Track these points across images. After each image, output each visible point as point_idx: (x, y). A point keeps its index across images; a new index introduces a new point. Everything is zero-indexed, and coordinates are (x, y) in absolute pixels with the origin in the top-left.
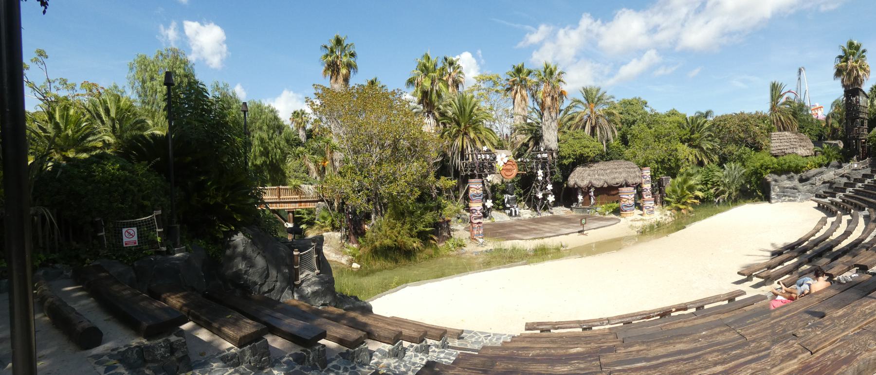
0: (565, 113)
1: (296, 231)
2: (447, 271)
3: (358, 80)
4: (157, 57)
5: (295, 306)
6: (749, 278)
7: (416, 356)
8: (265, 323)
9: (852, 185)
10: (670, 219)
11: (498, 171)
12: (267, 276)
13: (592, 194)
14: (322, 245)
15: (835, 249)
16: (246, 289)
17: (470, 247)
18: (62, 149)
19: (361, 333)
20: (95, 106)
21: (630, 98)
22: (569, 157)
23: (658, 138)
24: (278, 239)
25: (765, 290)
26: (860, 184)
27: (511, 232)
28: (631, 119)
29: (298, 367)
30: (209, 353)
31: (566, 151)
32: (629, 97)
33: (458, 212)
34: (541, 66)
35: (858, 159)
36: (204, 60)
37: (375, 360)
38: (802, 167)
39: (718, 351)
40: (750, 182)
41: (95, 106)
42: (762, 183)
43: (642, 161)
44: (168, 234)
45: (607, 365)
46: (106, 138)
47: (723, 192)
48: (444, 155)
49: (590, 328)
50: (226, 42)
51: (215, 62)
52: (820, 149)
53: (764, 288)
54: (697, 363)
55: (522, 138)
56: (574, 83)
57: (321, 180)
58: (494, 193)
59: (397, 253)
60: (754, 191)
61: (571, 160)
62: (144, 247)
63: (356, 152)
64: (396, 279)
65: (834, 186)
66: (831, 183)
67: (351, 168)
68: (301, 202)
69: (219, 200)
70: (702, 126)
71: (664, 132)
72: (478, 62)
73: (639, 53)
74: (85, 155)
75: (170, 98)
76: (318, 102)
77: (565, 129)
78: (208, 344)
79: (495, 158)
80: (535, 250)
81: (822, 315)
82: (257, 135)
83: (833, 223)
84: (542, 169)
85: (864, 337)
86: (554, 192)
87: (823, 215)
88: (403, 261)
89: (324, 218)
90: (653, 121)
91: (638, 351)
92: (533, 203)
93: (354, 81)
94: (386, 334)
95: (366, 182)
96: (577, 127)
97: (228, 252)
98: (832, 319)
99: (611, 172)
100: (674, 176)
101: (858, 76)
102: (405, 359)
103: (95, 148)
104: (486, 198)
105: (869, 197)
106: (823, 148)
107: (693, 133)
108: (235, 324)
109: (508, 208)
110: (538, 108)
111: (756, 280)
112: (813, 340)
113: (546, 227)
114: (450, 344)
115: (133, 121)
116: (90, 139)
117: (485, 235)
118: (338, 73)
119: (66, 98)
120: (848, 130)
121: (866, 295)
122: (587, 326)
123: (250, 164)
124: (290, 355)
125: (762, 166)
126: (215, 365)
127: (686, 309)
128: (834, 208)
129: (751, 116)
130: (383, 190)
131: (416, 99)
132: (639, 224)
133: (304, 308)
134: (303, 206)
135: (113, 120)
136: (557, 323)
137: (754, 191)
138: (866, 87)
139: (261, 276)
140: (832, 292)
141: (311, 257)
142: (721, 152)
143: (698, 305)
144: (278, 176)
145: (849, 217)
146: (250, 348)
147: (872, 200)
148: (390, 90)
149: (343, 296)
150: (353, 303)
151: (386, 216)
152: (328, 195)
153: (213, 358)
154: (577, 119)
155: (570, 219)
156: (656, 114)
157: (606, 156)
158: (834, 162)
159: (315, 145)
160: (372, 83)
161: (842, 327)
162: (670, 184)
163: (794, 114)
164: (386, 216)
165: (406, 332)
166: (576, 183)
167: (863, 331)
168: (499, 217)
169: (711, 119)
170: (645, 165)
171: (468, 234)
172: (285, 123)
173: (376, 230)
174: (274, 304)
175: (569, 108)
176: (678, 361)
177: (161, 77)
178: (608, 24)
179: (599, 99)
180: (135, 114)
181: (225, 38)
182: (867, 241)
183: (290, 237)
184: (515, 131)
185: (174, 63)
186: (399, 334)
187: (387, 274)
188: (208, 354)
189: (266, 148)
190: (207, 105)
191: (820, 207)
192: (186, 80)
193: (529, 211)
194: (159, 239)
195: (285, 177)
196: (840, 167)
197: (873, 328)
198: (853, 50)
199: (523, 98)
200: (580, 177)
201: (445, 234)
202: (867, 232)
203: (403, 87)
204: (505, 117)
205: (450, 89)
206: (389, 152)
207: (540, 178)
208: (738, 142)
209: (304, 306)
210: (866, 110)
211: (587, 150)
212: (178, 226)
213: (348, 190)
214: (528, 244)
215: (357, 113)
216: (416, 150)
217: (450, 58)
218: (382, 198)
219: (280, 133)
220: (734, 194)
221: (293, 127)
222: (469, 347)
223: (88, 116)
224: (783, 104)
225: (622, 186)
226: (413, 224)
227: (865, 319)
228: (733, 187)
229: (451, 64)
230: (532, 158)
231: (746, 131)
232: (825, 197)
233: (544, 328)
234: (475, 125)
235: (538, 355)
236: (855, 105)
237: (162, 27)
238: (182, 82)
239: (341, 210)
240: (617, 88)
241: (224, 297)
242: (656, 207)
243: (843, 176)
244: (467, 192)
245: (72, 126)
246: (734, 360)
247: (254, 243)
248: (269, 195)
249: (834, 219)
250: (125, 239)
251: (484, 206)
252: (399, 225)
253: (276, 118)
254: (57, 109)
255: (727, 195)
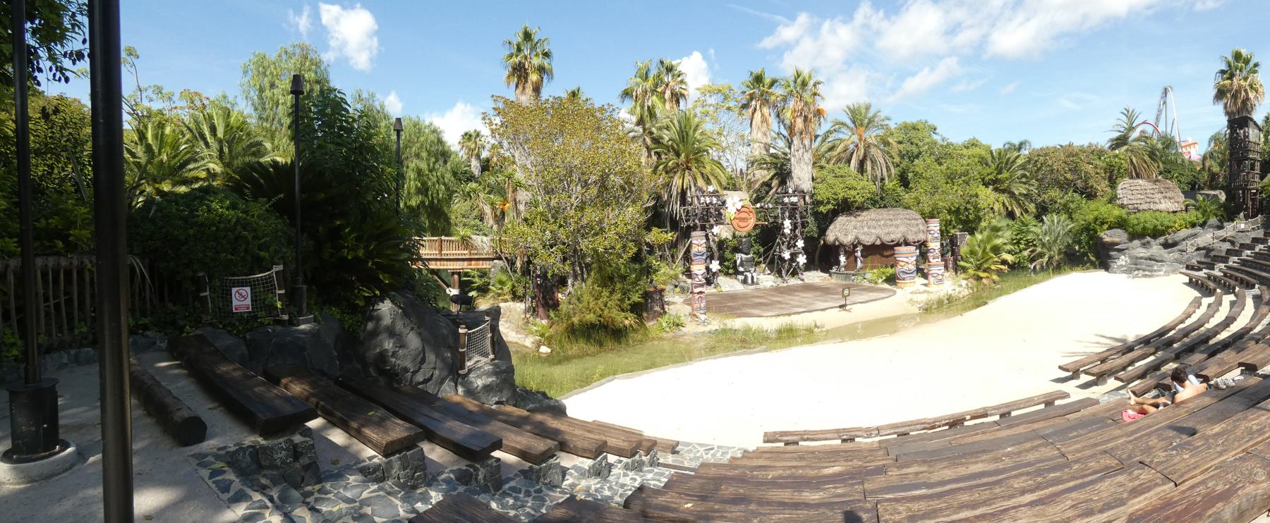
0: (824, 140)
1: (463, 300)
2: (658, 360)
3: (552, 91)
4: (280, 56)
5: (458, 404)
6: (1076, 374)
7: (625, 475)
8: (420, 426)
9: (1237, 253)
10: (966, 292)
11: (728, 221)
12: (423, 361)
13: (859, 254)
14: (498, 320)
15: (1211, 342)
16: (393, 376)
17: (690, 328)
18: (155, 180)
19: (550, 443)
20: (197, 122)
21: (915, 121)
22: (828, 203)
23: (951, 178)
24: (438, 311)
25: (1095, 392)
26: (1249, 252)
27: (745, 306)
28: (916, 151)
29: (461, 489)
30: (344, 464)
31: (824, 194)
32: (912, 119)
33: (676, 277)
34: (790, 73)
35: (1246, 217)
36: (347, 59)
37: (569, 481)
38: (1168, 227)
39: (1028, 474)
40: (1079, 243)
41: (197, 122)
42: (1096, 244)
43: (927, 210)
44: (291, 298)
45: (873, 492)
46: (211, 166)
47: (1041, 255)
48: (658, 197)
49: (852, 440)
50: (377, 33)
51: (362, 60)
52: (1193, 202)
53: (1095, 388)
54: (997, 490)
55: (763, 175)
56: (836, 100)
57: (499, 229)
58: (722, 252)
59: (602, 333)
60: (1085, 254)
61: (830, 206)
62: (260, 314)
63: (549, 192)
64: (601, 368)
65: (1212, 254)
66: (1208, 250)
67: (542, 214)
68: (470, 260)
69: (361, 253)
70: (1014, 162)
71: (960, 170)
72: (710, 67)
73: (932, 59)
74: (183, 189)
75: (297, 111)
76: (498, 120)
77: (823, 163)
78: (343, 450)
79: (724, 203)
80: (779, 332)
81: (1193, 433)
82: (412, 165)
83: (1209, 305)
84: (790, 218)
85: (1250, 464)
86: (806, 250)
87: (1196, 294)
88: (609, 344)
89: (501, 283)
90: (944, 154)
91: (917, 474)
92: (776, 266)
93: (548, 92)
94: (586, 445)
95: (562, 234)
96: (839, 160)
97: (370, 326)
98: (1206, 438)
99: (885, 225)
100: (972, 233)
101: (1248, 99)
102: (611, 478)
103: (197, 179)
104: (711, 258)
105: (1261, 270)
106: (1197, 201)
107: (1000, 172)
108: (380, 424)
109: (742, 273)
110: (785, 133)
111: (1084, 378)
112: (1177, 467)
113: (795, 299)
114: (661, 461)
115: (245, 143)
116: (191, 166)
117: (708, 309)
118: (526, 81)
119: (161, 112)
120: (1232, 176)
121: (1253, 406)
122: (848, 437)
123: (402, 205)
124: (451, 471)
125: (1096, 219)
126: (352, 478)
127: (985, 415)
128: (1212, 285)
129: (1082, 150)
130: (584, 245)
131: (634, 119)
132: (923, 298)
133: (472, 408)
134: (474, 265)
135: (220, 142)
136: (805, 432)
137: (1085, 254)
138: (1258, 116)
139: (414, 360)
140: (1207, 400)
141: (484, 337)
142: (1040, 200)
143: (1002, 411)
144: (439, 222)
145: (1232, 297)
146: (400, 459)
147: (1264, 274)
148: (597, 106)
149: (527, 392)
150: (540, 401)
151: (590, 281)
152: (508, 250)
153: (349, 469)
154: (839, 149)
155: (828, 289)
156: (949, 145)
157: (879, 201)
158: (1213, 220)
159: (492, 180)
160: (574, 94)
161: (1219, 449)
162: (966, 243)
163: (1152, 154)
164: (590, 281)
165: (612, 442)
166: (837, 239)
167: (1248, 455)
168: (728, 285)
169: (1027, 152)
170: (932, 217)
171: (688, 309)
172: (453, 149)
173: (574, 300)
174: (430, 400)
175: (830, 132)
176: (971, 488)
177: (285, 84)
178: (893, 18)
179: (870, 121)
180: (248, 134)
181: (376, 27)
182: (1256, 330)
183: (454, 308)
184: (753, 163)
185: (302, 64)
186: (599, 445)
187: (589, 362)
188: (342, 464)
189: (424, 184)
190: (347, 122)
191: (1193, 283)
192: (317, 88)
193: (771, 277)
194: (279, 305)
195: (449, 224)
196: (1220, 227)
197: (1261, 452)
198: (1238, 64)
199: (764, 120)
200: (842, 231)
201: (657, 308)
202: (1257, 317)
203: (616, 102)
204: (739, 145)
205: (668, 106)
206: (594, 191)
207: (787, 231)
208: (1064, 186)
209: (471, 405)
210: (1257, 148)
211: (853, 192)
212: (305, 287)
213: (537, 244)
214: (768, 323)
215: (551, 136)
216: (629, 190)
217: (667, 62)
218: (584, 256)
219: (445, 162)
220: (1057, 257)
221: (463, 154)
222: (686, 465)
223: (188, 136)
224: (1137, 140)
225: (898, 245)
226: (625, 293)
227: (1251, 439)
228: (1056, 249)
229: (670, 69)
230: (777, 203)
231: (1074, 170)
232: (1200, 269)
233: (791, 439)
234: (697, 156)
235: (781, 477)
236: (1243, 141)
237: (291, 12)
238: (312, 90)
239: (526, 272)
240: (896, 109)
241: (363, 388)
242: (947, 274)
243: (1224, 240)
244: (688, 251)
245: (168, 149)
246: (1052, 486)
247: (406, 314)
248: (428, 248)
249: (1211, 300)
250: (235, 302)
251: (708, 269)
252: (606, 293)
253: (440, 141)
254: (150, 126)
255: (1046, 259)
